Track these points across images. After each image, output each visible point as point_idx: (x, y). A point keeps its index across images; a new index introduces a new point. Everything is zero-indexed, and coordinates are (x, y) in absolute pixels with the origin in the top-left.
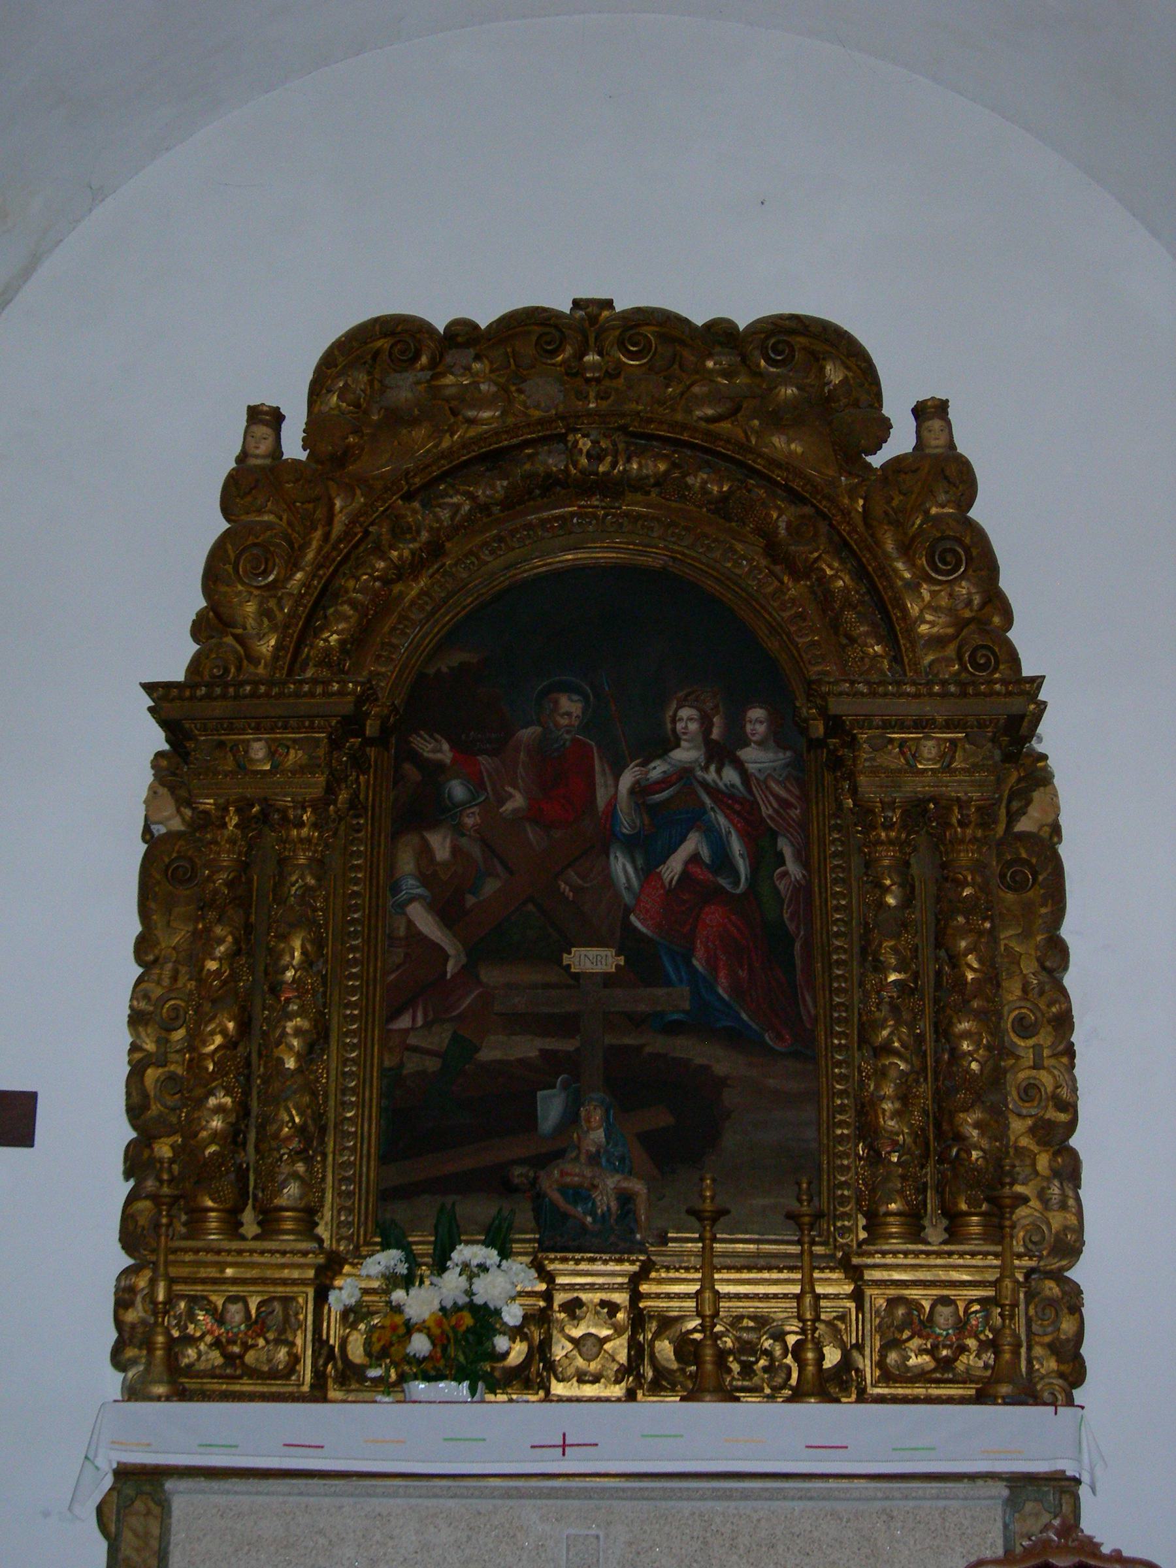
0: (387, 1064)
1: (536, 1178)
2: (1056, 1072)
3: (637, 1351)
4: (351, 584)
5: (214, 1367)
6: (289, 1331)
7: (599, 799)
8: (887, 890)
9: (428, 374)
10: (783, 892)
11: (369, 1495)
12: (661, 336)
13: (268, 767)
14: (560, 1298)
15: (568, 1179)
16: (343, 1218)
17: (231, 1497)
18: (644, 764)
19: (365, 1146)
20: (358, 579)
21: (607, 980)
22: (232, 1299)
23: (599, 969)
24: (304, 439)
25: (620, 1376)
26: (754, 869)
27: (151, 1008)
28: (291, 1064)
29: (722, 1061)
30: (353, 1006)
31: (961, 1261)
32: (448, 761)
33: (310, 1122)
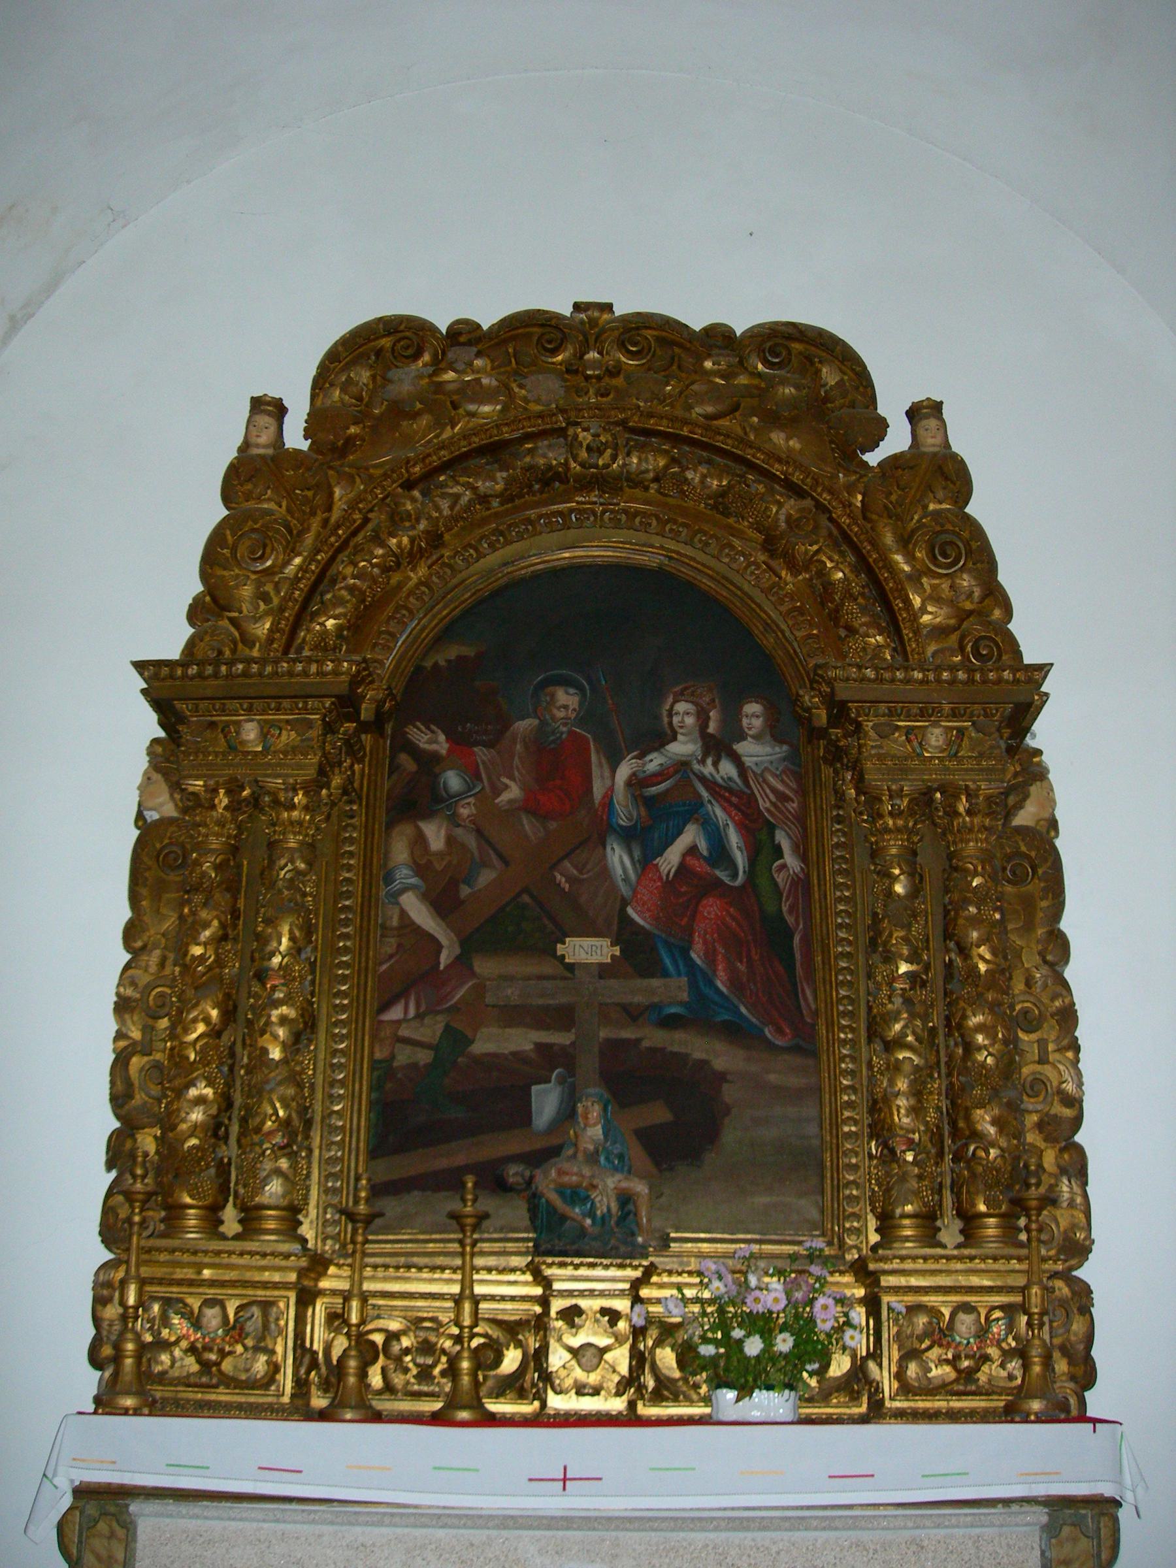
0: (378, 1055)
1: (532, 1178)
2: (1061, 1067)
3: (639, 1359)
4: (349, 570)
5: (189, 1375)
6: (268, 1338)
7: (595, 789)
8: (895, 879)
9: (431, 370)
10: (781, 885)
11: (351, 1524)
12: (658, 339)
13: (260, 749)
14: (557, 1305)
15: (566, 1179)
16: (328, 1216)
17: (199, 1522)
18: (641, 756)
19: (354, 1140)
20: (355, 565)
21: (604, 971)
22: (209, 1303)
23: (595, 959)
24: (306, 429)
25: (621, 1389)
26: (752, 861)
27: (138, 996)
28: (276, 1054)
29: (722, 1056)
30: (345, 994)
31: (983, 1266)
32: (444, 752)
33: (294, 1115)
